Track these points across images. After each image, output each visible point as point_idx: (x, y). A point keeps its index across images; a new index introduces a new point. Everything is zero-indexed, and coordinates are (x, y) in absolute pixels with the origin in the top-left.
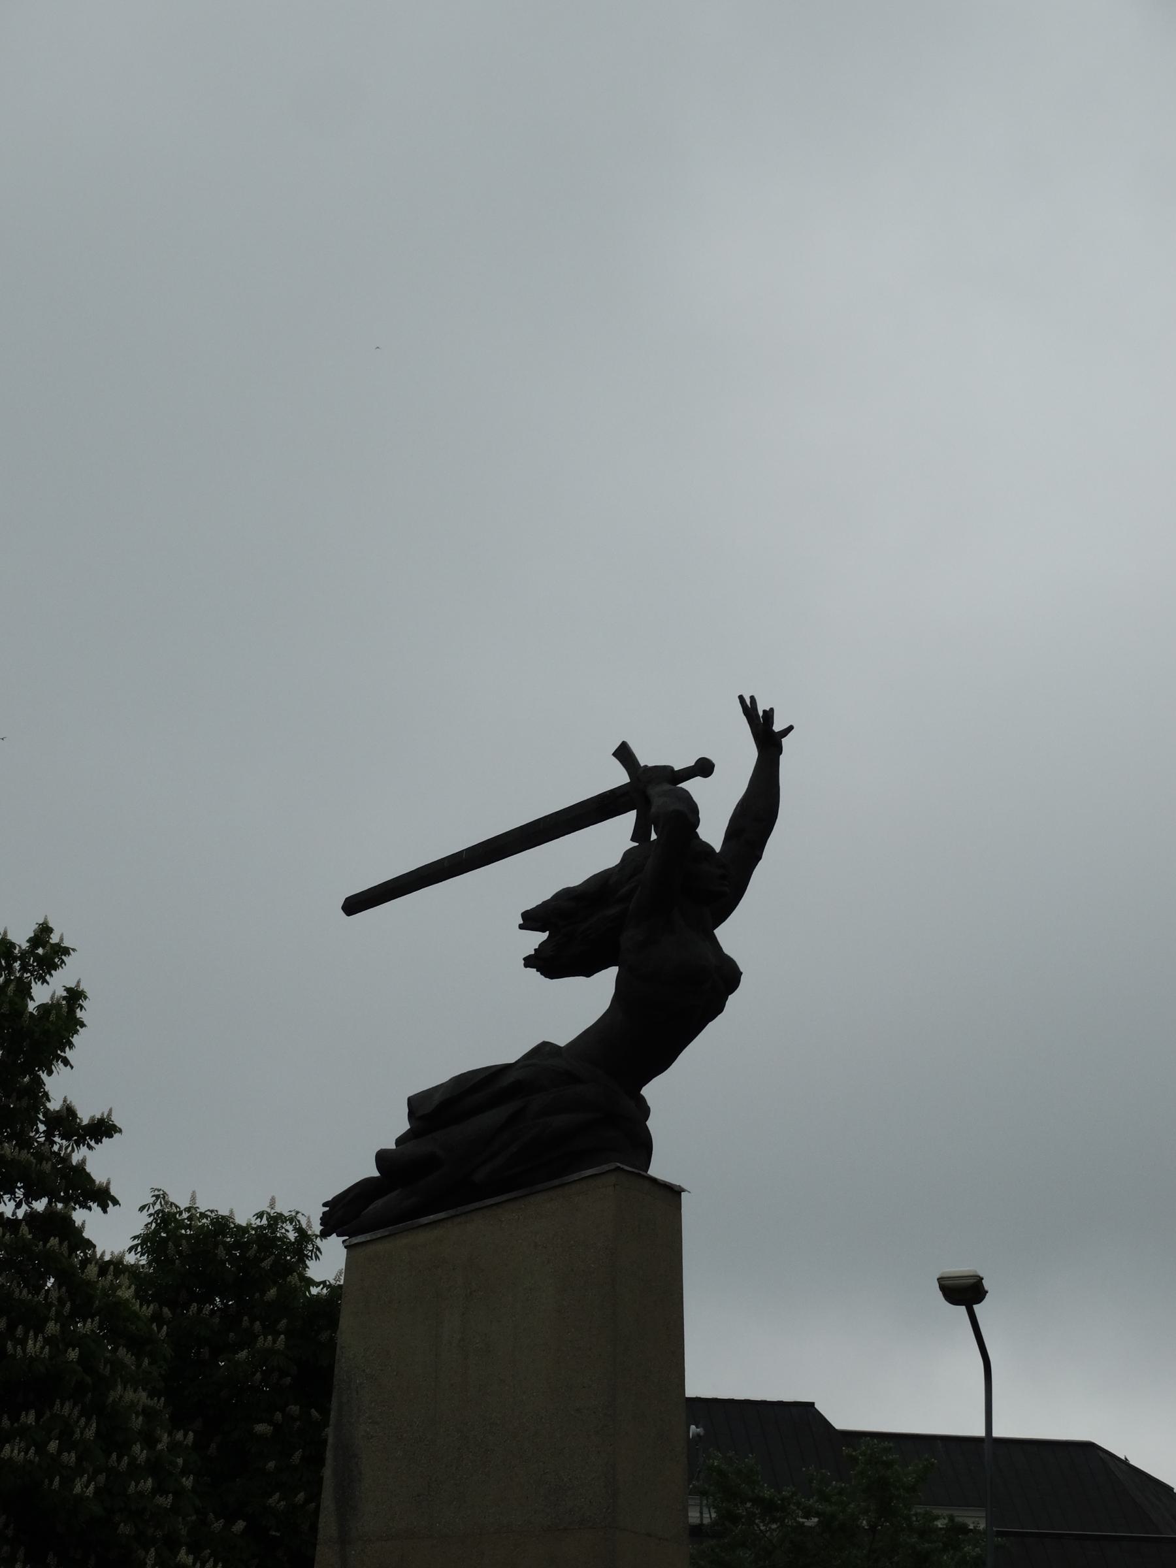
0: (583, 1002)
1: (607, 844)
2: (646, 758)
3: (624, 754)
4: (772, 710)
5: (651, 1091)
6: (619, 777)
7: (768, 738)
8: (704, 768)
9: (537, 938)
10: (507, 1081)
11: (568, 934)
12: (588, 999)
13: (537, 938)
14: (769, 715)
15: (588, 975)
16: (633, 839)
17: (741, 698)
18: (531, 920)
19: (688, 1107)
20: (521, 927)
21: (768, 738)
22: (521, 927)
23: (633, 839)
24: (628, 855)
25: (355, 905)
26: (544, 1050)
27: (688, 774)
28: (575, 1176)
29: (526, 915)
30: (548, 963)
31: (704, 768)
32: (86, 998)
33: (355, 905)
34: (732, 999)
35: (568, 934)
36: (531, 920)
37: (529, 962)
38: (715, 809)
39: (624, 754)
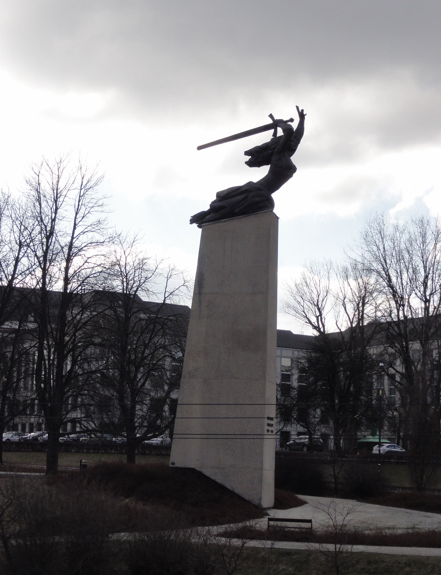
0: (260, 173)
1: (266, 137)
2: (276, 118)
3: (271, 116)
5: (275, 196)
6: (271, 122)
7: (302, 115)
8: (292, 120)
9: (248, 158)
10: (242, 190)
11: (256, 157)
12: (260, 173)
13: (248, 158)
14: (303, 110)
17: (297, 108)
18: (247, 153)
19: (283, 199)
20: (190, 224)
22: (190, 224)
24: (272, 139)
25: (200, 148)
26: (250, 183)
28: (261, 212)
30: (250, 164)
32: (247, 163)
33: (200, 148)
35: (256, 157)
36: (247, 153)
38: (295, 125)
39: (271, 116)
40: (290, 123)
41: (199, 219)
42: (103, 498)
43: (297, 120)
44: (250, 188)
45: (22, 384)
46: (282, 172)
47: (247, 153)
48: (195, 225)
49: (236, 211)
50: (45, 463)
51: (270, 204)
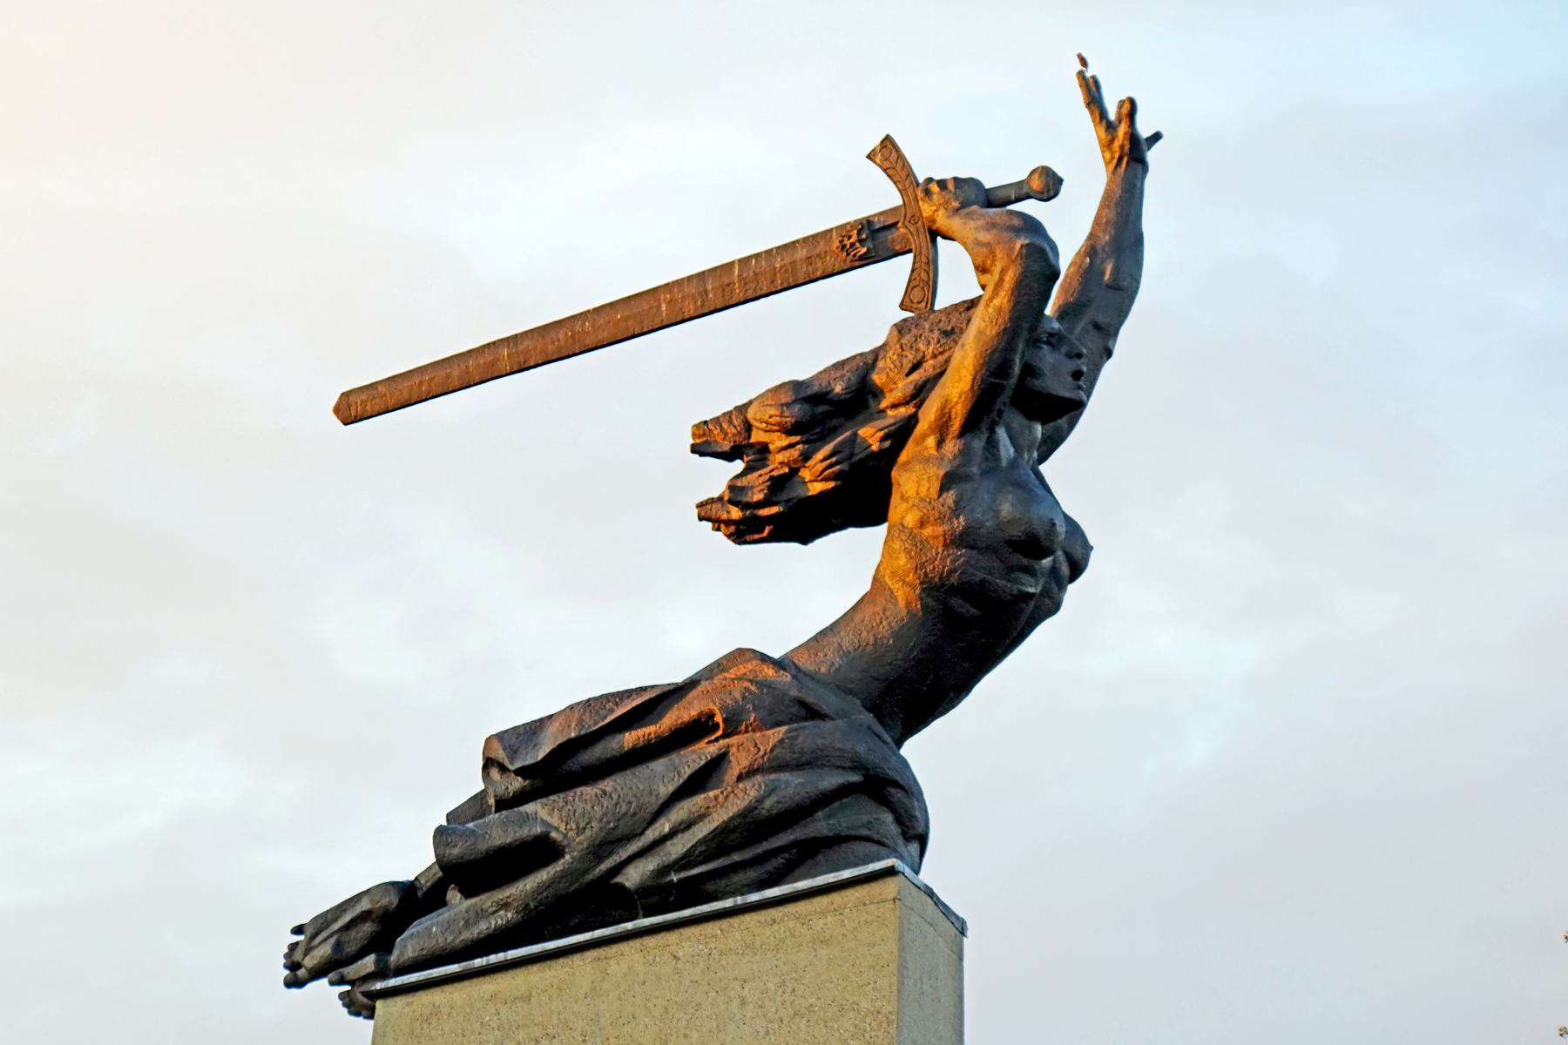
0: (820, 588)
1: (850, 318)
4: (888, 138)
6: (878, 196)
7: (1130, 153)
8: (1048, 185)
9: (719, 475)
11: (801, 467)
12: (820, 588)
13: (719, 475)
14: (1130, 109)
15: (805, 542)
16: (903, 306)
21: (1130, 153)
23: (903, 306)
27: (1021, 192)
29: (702, 429)
30: (746, 521)
31: (1048, 185)
34: (1074, 593)
35: (801, 467)
37: (707, 512)
39: (888, 155)
40: (1029, 207)
48: (324, 992)
49: (632, 877)
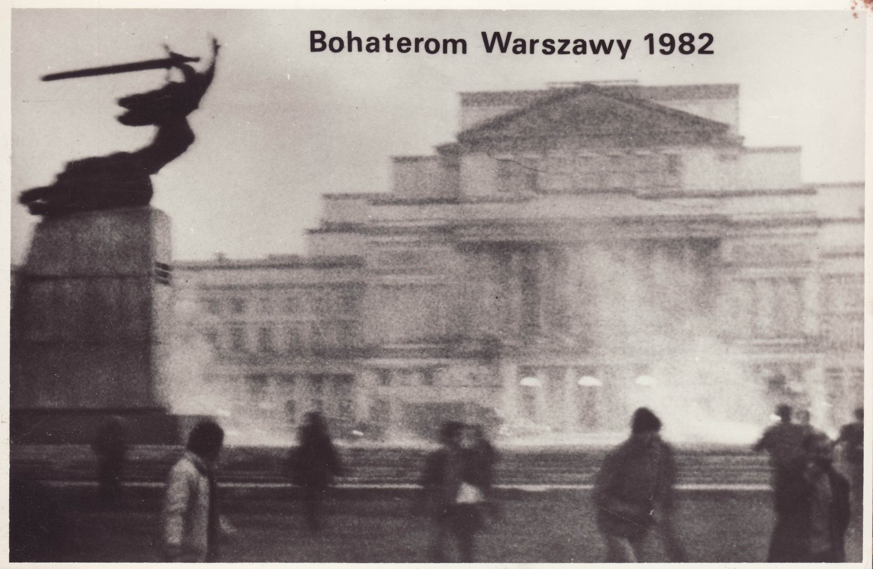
0: (141, 137)
1: (151, 81)
7: (216, 47)
9: (122, 110)
11: (135, 110)
12: (141, 137)
13: (122, 110)
25: (49, 78)
30: (125, 120)
33: (49, 78)
35: (135, 110)
41: (30, 199)
42: (356, 522)
43: (206, 53)
44: (120, 158)
45: (675, 189)
46: (174, 141)
47: (123, 102)
50: (767, 476)
51: (147, 192)
